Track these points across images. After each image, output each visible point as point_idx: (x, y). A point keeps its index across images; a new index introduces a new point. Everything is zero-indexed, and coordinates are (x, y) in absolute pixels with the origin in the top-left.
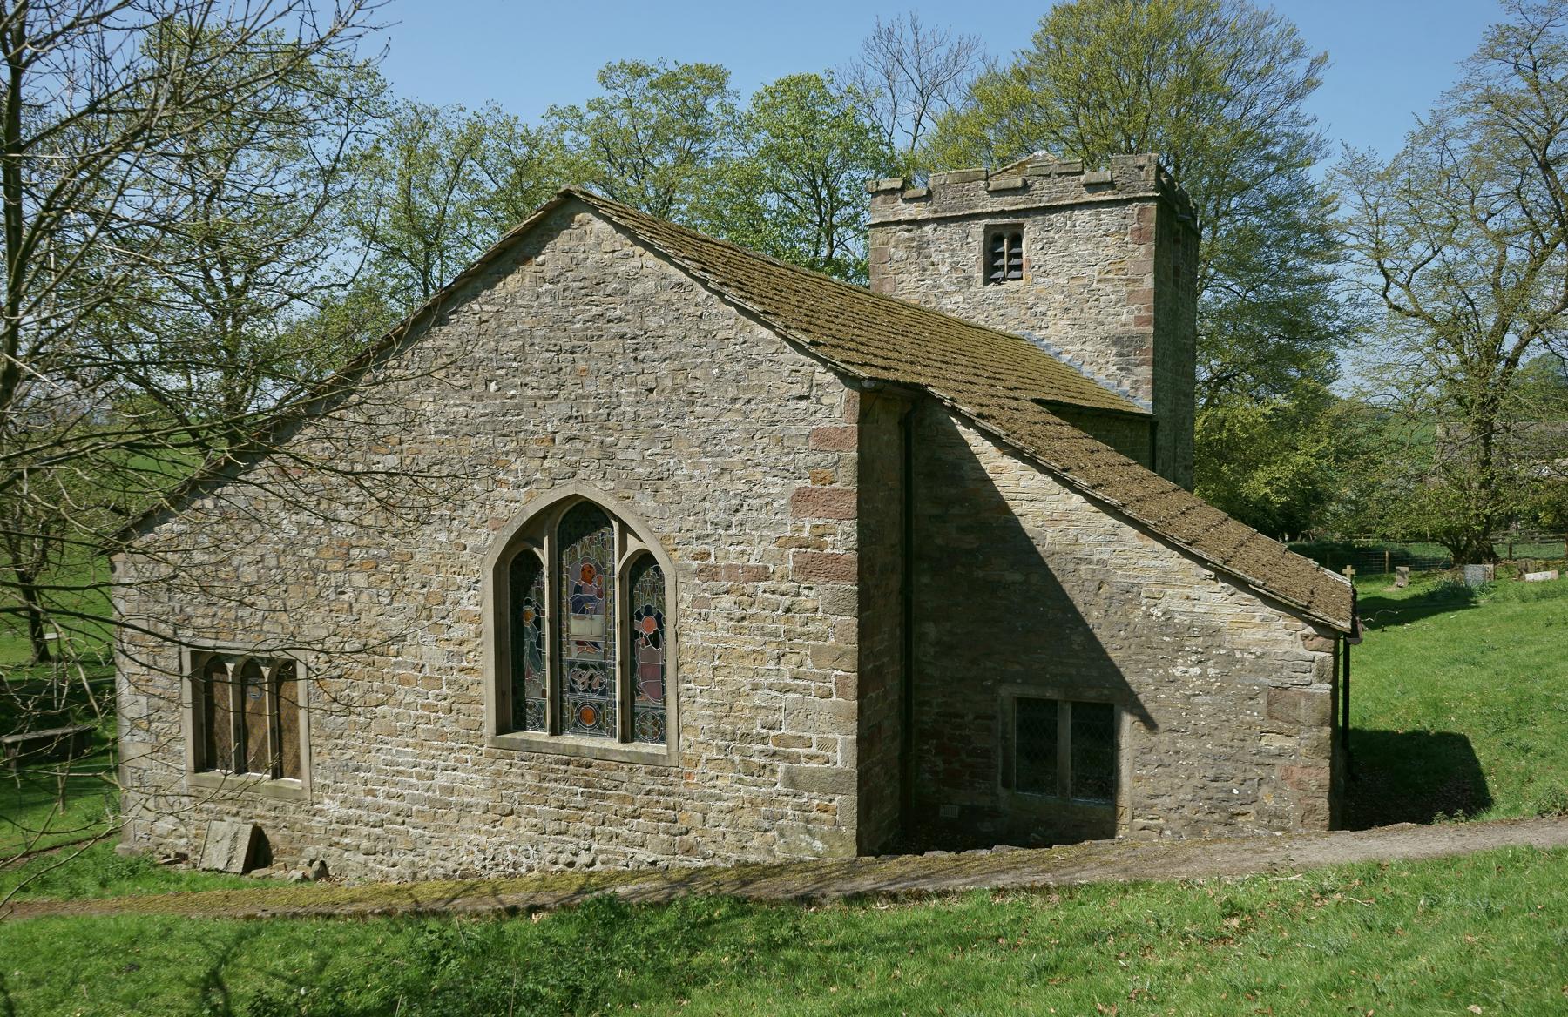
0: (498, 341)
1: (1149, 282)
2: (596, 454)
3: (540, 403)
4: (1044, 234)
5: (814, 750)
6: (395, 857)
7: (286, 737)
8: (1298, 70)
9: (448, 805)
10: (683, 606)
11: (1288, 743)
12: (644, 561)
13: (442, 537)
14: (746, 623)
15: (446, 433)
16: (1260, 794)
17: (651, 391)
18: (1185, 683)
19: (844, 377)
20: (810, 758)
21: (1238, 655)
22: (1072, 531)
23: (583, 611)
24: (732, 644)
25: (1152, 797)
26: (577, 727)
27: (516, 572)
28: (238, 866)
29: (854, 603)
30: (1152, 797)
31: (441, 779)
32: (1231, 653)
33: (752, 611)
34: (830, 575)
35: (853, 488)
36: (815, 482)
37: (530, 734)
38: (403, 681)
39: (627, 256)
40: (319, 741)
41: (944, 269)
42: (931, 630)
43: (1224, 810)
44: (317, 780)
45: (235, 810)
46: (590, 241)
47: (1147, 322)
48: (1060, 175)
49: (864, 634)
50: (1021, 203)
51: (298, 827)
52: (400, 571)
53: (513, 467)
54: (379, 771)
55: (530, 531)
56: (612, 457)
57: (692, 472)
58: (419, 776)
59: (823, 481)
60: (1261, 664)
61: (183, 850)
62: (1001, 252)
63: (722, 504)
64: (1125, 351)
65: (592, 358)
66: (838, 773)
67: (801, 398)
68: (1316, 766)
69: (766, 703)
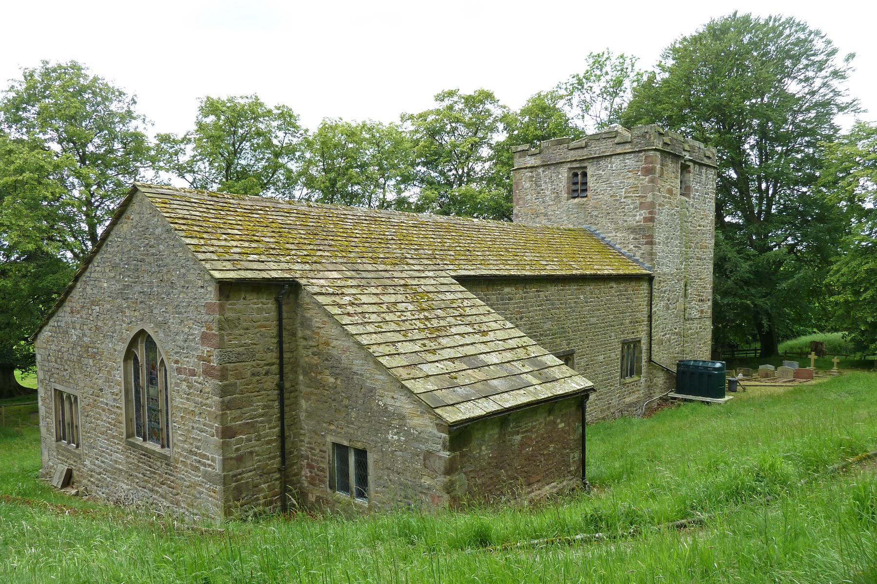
18: (392, 444)
32: (408, 431)
34: (212, 376)
41: (548, 193)
57: (173, 322)
60: (418, 439)
64: (637, 237)
66: (217, 475)
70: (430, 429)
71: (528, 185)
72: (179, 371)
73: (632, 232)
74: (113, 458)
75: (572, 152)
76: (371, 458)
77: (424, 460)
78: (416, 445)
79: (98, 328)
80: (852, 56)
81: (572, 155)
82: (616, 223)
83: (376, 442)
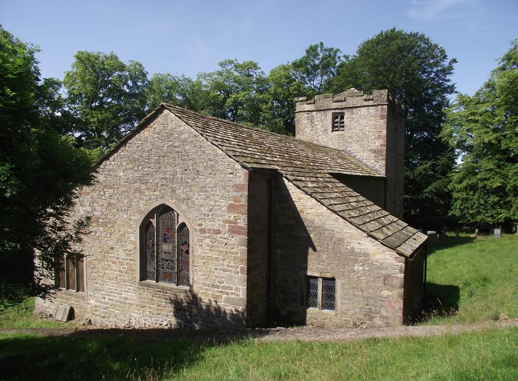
0: (142, 153)
1: (384, 132)
2: (170, 191)
3: (154, 173)
4: (351, 116)
5: (233, 291)
6: (111, 319)
7: (81, 278)
8: (446, 63)
9: (125, 303)
10: (195, 242)
11: (390, 293)
12: (183, 225)
13: (125, 216)
14: (213, 248)
15: (127, 182)
16: (381, 311)
17: (186, 170)
18: (358, 272)
19: (243, 167)
20: (232, 294)
21: (375, 263)
22: (323, 220)
23: (166, 242)
24: (209, 255)
25: (347, 310)
26: (164, 280)
27: (145, 227)
28: (65, 320)
29: (246, 243)
30: (347, 310)
31: (124, 295)
33: (215, 244)
34: (239, 233)
35: (246, 204)
36: (235, 202)
37: (148, 281)
38: (114, 263)
39: (180, 126)
40: (89, 281)
42: (279, 251)
43: (370, 315)
44: (89, 293)
45: (66, 301)
46: (169, 121)
47: (384, 146)
48: (356, 96)
49: (250, 252)
50: (343, 104)
51: (83, 308)
52: (113, 227)
53: (146, 194)
54: (106, 291)
55: (150, 215)
56: (174, 191)
57: (198, 198)
58: (118, 293)
59: (237, 201)
60: (381, 267)
61: (51, 313)
62: (338, 122)
63: (206, 208)
65: (169, 159)
67: (231, 173)
68: (398, 301)
69: (220, 276)
70: (390, 261)
71: (306, 122)
72: (203, 231)
73: (373, 153)
74: (123, 296)
75: (335, 103)
76: (338, 284)
77: (384, 280)
78: (378, 271)
79: (110, 204)
80: (454, 61)
81: (335, 105)
82: (364, 147)
83: (344, 272)
